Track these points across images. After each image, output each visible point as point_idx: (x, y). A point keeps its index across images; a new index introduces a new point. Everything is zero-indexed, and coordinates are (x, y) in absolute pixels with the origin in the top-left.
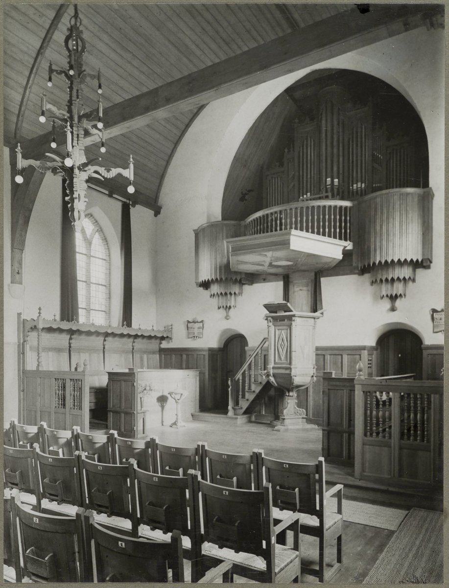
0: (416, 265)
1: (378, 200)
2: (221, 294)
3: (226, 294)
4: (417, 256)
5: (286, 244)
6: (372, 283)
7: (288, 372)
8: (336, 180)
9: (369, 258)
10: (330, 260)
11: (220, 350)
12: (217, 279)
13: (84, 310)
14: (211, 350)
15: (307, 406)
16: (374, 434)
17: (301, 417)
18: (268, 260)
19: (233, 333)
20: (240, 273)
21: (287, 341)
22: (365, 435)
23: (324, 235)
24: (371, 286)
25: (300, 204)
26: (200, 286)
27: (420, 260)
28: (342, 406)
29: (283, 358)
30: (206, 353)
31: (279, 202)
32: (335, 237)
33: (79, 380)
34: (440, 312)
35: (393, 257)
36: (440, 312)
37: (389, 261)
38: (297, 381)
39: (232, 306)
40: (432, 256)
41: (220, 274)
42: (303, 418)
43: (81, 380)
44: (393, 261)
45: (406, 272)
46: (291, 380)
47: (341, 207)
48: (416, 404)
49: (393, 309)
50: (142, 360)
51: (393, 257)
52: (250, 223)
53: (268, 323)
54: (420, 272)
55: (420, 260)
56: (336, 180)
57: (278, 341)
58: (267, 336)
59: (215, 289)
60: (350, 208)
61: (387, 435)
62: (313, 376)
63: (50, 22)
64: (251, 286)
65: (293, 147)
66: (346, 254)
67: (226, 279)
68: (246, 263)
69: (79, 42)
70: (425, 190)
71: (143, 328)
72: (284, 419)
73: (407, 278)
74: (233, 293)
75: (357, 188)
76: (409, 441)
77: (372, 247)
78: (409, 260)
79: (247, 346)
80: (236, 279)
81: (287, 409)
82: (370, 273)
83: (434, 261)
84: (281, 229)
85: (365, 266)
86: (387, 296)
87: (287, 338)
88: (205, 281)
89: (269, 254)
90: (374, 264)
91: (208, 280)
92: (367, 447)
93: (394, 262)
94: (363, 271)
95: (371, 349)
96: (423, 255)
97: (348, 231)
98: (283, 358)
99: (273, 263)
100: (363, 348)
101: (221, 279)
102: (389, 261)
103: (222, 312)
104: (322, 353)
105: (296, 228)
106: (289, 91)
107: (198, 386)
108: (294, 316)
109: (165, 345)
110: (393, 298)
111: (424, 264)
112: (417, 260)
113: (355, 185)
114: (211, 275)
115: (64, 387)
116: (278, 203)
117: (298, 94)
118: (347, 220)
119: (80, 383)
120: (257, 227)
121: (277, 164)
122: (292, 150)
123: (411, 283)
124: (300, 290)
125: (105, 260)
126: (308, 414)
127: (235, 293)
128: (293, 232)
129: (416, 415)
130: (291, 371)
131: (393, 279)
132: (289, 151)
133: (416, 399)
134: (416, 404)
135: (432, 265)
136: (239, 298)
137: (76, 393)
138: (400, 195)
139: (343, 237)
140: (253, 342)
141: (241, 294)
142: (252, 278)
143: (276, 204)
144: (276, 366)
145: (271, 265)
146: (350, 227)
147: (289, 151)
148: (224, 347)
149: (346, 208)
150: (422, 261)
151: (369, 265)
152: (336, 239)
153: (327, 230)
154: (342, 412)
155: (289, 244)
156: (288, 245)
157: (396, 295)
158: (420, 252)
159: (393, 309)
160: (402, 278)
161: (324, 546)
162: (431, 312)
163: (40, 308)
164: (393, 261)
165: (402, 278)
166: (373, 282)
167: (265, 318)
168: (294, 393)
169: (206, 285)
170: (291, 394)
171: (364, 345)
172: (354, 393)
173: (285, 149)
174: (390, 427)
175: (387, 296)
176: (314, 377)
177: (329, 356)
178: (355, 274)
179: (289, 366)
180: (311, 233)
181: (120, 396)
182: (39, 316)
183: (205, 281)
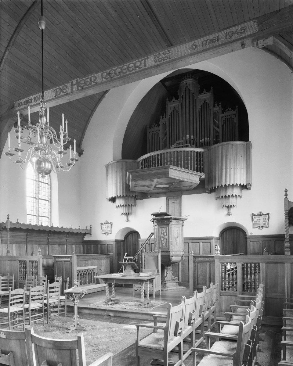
0: (244, 187)
1: (220, 147)
2: (123, 205)
3: (129, 205)
4: (244, 182)
5: (166, 174)
6: (217, 198)
7: (168, 254)
8: (192, 136)
9: (219, 182)
10: (192, 184)
11: (123, 241)
12: (120, 196)
13: (35, 217)
14: (116, 241)
15: (178, 275)
16: (227, 289)
17: (176, 282)
18: (154, 184)
19: (131, 230)
20: (135, 192)
21: (167, 234)
22: (222, 289)
23: (188, 168)
24: (216, 200)
25: (172, 150)
26: (109, 201)
27: (245, 185)
28: (205, 273)
29: (164, 245)
30: (114, 243)
31: (157, 149)
32: (194, 170)
33: (36, 261)
34: (256, 215)
35: (229, 182)
36: (256, 215)
37: (227, 185)
38: (174, 259)
39: (130, 213)
40: (251, 182)
41: (123, 193)
42: (176, 282)
43: (37, 261)
44: (233, 184)
45: (237, 191)
46: (170, 259)
47: (197, 152)
48: (251, 269)
49: (229, 214)
50: (72, 249)
51: (229, 182)
52: (141, 161)
53: (154, 224)
54: (245, 191)
55: (245, 185)
56: (192, 136)
57: (161, 235)
58: (153, 232)
59: (119, 202)
60: (203, 152)
61: (235, 289)
62: (182, 256)
63: (14, 29)
64: (142, 201)
65: (166, 115)
66: (202, 181)
67: (126, 196)
68: (141, 186)
69: (235, 38)
70: (248, 143)
71: (73, 228)
72: (165, 283)
73: (237, 195)
74: (130, 205)
75: (205, 141)
76: (247, 292)
77: (217, 176)
78: (239, 184)
79: (140, 238)
80: (133, 196)
81: (167, 277)
82: (215, 192)
83: (252, 185)
84: (161, 165)
85: (212, 188)
86: (226, 206)
87: (166, 233)
88: (113, 197)
89: (156, 180)
90: (218, 186)
91: (115, 197)
92: (223, 297)
93: (226, 186)
94: (212, 190)
95: (217, 239)
96: (247, 181)
97: (202, 167)
98: (164, 245)
99: (157, 186)
100: (212, 238)
101: (123, 196)
102: (227, 185)
103: (125, 217)
104: (187, 241)
105: (174, 165)
106: (163, 81)
107: (109, 265)
108: (171, 218)
109: (86, 238)
110: (229, 207)
111: (247, 187)
112: (243, 185)
113: (203, 139)
114: (120, 193)
115: (25, 266)
116: (154, 149)
117: (167, 83)
118: (201, 160)
119: (36, 263)
120: (143, 165)
121: (156, 125)
122: (164, 116)
123: (238, 198)
124: (173, 203)
125: (48, 184)
126: (179, 280)
127: (132, 205)
128: (171, 167)
129: (251, 277)
130: (170, 253)
131: (229, 196)
132: (163, 118)
133: (251, 267)
134: (251, 269)
135: (252, 188)
136: (134, 208)
137: (33, 270)
138: (233, 145)
139: (199, 170)
140: (144, 235)
141: (135, 205)
142: (144, 195)
143: (152, 151)
144: (209, 241)
145: (155, 187)
146: (203, 164)
147: (163, 118)
148: (125, 238)
149: (201, 152)
150: (246, 185)
151: (215, 187)
152: (198, 172)
153: (189, 166)
154: (205, 277)
155: (168, 174)
156: (167, 175)
157: (231, 205)
158: (245, 180)
159: (229, 214)
160: (234, 195)
161: (291, 332)
162: (252, 216)
163: (8, 215)
164: (233, 184)
165: (234, 195)
166: (217, 197)
167: (153, 220)
168: (171, 267)
169: (113, 200)
170: (169, 268)
171: (213, 236)
172: (214, 266)
173: (160, 116)
174: (236, 283)
175: (226, 206)
176: (183, 257)
177: (191, 243)
178: (206, 193)
179: (168, 250)
180: (180, 167)
181: (62, 271)
182: (8, 220)
183: (113, 197)
